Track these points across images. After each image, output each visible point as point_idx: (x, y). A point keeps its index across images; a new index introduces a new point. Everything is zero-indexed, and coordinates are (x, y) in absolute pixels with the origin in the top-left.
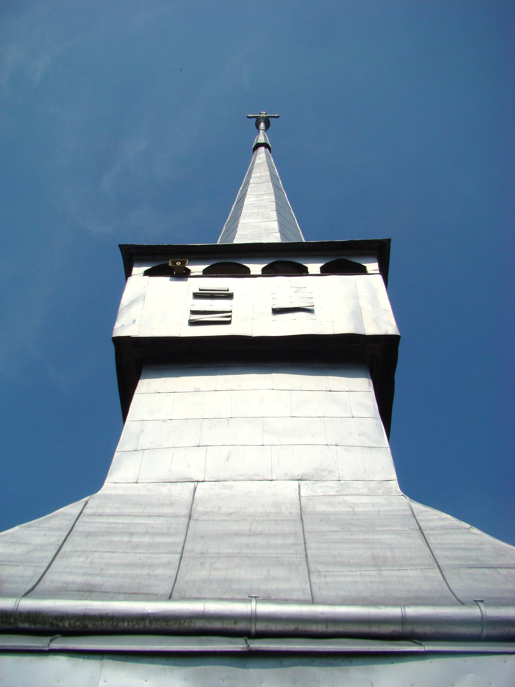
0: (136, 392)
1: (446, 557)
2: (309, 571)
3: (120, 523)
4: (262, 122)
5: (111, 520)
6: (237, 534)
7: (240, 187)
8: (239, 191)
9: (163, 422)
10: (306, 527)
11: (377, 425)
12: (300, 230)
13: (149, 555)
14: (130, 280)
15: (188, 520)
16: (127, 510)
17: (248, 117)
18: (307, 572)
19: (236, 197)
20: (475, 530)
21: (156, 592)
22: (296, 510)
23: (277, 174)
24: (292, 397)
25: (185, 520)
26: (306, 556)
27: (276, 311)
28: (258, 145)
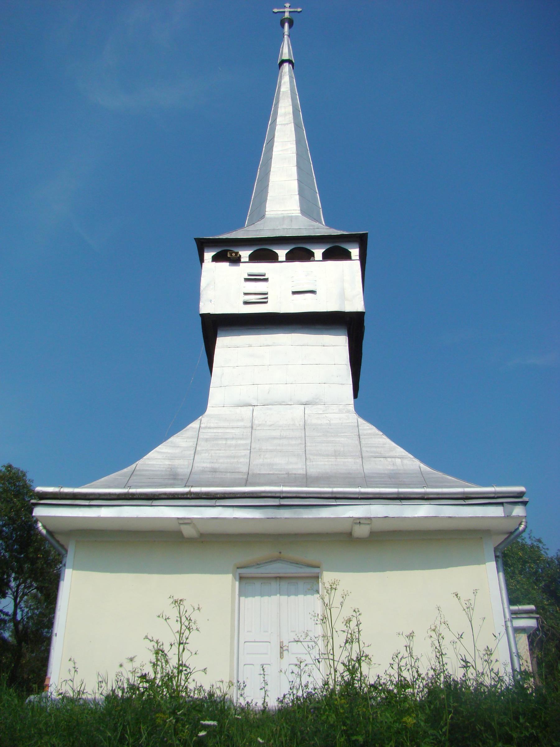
0: (216, 347)
1: (367, 451)
5: (215, 431)
6: (274, 438)
8: (269, 125)
9: (233, 368)
10: (306, 433)
13: (236, 451)
14: (204, 265)
16: (222, 424)
18: (305, 459)
20: (384, 437)
21: (242, 471)
22: (302, 423)
25: (250, 430)
26: (305, 451)
27: (294, 293)
28: (283, 62)
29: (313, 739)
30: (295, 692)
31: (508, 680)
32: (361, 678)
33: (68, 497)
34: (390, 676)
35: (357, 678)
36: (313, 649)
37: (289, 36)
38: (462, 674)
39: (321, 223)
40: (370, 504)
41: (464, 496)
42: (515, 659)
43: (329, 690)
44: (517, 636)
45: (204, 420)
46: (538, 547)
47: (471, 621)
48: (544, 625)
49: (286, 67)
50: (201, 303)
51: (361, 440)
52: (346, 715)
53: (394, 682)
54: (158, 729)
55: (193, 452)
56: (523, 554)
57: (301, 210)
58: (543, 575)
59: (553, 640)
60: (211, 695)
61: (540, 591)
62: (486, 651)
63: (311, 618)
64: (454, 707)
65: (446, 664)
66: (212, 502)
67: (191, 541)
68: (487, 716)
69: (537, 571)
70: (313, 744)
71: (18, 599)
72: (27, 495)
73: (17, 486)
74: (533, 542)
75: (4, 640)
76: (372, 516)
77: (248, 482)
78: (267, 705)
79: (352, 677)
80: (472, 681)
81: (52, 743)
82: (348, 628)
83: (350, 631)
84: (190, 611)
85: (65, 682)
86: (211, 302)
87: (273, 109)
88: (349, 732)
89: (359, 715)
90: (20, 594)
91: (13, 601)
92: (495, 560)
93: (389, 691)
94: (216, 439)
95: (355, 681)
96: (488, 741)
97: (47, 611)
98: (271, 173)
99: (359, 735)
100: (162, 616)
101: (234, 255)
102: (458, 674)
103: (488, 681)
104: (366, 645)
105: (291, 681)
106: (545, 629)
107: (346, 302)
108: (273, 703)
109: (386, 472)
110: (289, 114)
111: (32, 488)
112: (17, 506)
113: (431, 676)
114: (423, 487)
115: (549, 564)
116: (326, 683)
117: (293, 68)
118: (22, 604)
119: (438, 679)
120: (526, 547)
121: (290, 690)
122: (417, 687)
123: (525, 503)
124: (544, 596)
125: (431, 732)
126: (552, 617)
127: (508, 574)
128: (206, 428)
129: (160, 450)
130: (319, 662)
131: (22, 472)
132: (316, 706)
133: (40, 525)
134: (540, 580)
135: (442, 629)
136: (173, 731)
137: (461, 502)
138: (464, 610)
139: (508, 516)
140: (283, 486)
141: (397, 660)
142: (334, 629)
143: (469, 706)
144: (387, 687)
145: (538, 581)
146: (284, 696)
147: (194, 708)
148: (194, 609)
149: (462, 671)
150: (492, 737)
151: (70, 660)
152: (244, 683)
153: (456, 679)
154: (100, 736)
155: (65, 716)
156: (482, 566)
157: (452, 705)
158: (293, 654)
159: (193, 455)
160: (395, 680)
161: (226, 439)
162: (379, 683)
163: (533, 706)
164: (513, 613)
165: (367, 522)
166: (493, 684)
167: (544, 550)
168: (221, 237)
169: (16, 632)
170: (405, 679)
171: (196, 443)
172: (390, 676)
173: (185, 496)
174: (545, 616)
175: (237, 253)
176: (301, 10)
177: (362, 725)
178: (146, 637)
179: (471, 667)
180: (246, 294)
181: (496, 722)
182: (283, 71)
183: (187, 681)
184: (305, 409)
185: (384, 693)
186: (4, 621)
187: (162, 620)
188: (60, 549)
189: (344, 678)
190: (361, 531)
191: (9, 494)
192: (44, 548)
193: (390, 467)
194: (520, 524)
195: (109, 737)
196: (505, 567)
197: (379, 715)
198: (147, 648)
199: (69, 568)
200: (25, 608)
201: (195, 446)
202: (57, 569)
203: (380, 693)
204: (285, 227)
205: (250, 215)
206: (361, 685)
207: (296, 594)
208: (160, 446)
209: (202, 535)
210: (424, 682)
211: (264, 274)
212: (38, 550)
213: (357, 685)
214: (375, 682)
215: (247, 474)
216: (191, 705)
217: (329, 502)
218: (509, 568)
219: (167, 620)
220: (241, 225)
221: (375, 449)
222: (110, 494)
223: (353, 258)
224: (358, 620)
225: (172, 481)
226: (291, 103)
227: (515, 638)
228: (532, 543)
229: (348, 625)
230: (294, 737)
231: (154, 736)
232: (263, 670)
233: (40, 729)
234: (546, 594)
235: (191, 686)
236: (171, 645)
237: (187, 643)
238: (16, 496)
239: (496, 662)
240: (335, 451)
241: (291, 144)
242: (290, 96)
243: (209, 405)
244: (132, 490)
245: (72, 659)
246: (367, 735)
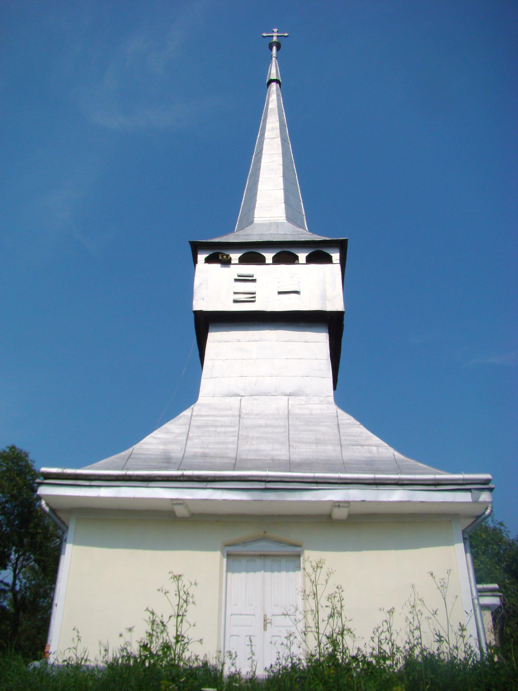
0: (207, 341)
2: (289, 446)
3: (210, 420)
4: (274, 46)
5: (206, 418)
6: (261, 426)
7: (258, 134)
8: (257, 139)
9: (223, 361)
10: (290, 422)
11: (328, 364)
12: (299, 187)
14: (198, 266)
15: (239, 418)
16: (213, 413)
18: (288, 447)
19: (255, 147)
20: (361, 426)
23: (284, 119)
25: (238, 418)
26: (289, 438)
27: (280, 293)
28: (271, 81)
36: (299, 622)
37: (277, 58)
39: (304, 229)
40: (349, 489)
41: (436, 482)
45: (196, 408)
46: (500, 530)
47: (444, 599)
48: (505, 602)
49: (274, 86)
50: (194, 301)
51: (340, 430)
55: (185, 438)
57: (287, 217)
58: (505, 556)
59: (514, 617)
60: (205, 664)
61: (502, 571)
63: (298, 594)
64: (431, 678)
66: (203, 485)
69: (499, 552)
71: (17, 571)
73: (20, 466)
74: (495, 525)
75: (3, 608)
76: (350, 500)
77: (236, 466)
80: (445, 654)
84: (188, 585)
86: (203, 300)
87: (261, 124)
90: (19, 566)
91: (12, 573)
92: (463, 542)
94: (206, 426)
98: (260, 183)
100: (162, 590)
101: (225, 257)
102: (432, 647)
104: (348, 619)
106: (506, 607)
107: (327, 302)
108: (261, 673)
109: (363, 459)
110: (276, 129)
112: (20, 484)
114: (398, 474)
115: (510, 546)
117: (280, 87)
118: (21, 576)
120: (489, 530)
121: (276, 660)
123: (491, 490)
124: (505, 575)
126: (513, 595)
128: (197, 416)
129: (155, 436)
131: (25, 453)
133: (43, 502)
138: (438, 588)
139: (476, 502)
140: (269, 471)
141: (377, 634)
145: (499, 561)
148: (191, 584)
149: (436, 645)
151: (74, 629)
152: (236, 653)
156: (451, 547)
158: (275, 626)
159: (186, 441)
160: (376, 652)
161: (216, 426)
163: (504, 679)
164: (479, 591)
165: (345, 505)
167: (505, 533)
168: (213, 241)
169: (15, 602)
170: (385, 651)
171: (188, 429)
173: (178, 479)
174: (507, 594)
175: (228, 256)
176: (288, 35)
178: (147, 609)
179: (445, 642)
180: (235, 293)
182: (271, 90)
184: (288, 400)
186: (4, 591)
187: (161, 594)
190: (340, 514)
191: (12, 473)
192: (44, 524)
193: (367, 455)
194: (487, 509)
197: (362, 685)
198: (446, 647)
199: (70, 543)
201: (188, 432)
204: (271, 232)
205: (239, 221)
207: (279, 571)
208: (155, 432)
209: (193, 515)
211: (252, 275)
212: (37, 526)
215: (235, 459)
220: (231, 230)
221: (352, 438)
222: (109, 476)
223: (334, 262)
224: (341, 596)
225: (166, 465)
226: (278, 119)
228: (494, 526)
232: (251, 641)
234: (507, 574)
238: (18, 475)
239: (470, 637)
240: (316, 439)
241: (277, 156)
242: (277, 112)
243: (201, 394)
244: (130, 473)
245: (76, 629)
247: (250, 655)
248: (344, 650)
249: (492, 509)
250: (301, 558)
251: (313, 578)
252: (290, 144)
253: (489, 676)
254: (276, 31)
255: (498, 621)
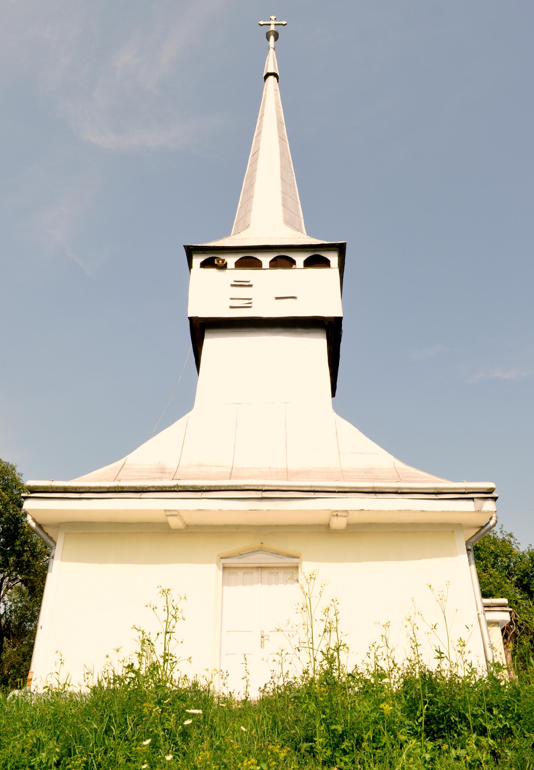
17: (260, 24)
24: (164, 610)
27: (277, 298)
28: (268, 75)
29: (294, 728)
30: (276, 680)
31: (482, 673)
32: (339, 668)
33: (59, 490)
34: (368, 665)
35: (335, 667)
38: (437, 666)
41: (436, 491)
42: (489, 650)
43: (309, 679)
44: (490, 630)
46: (510, 542)
47: (444, 612)
48: (517, 619)
52: (326, 703)
53: (372, 672)
54: (144, 719)
56: (495, 548)
60: (195, 684)
62: (459, 642)
65: (421, 655)
66: (198, 495)
67: (178, 532)
68: (461, 707)
70: (294, 733)
72: (15, 488)
78: (249, 695)
79: (331, 666)
80: (446, 672)
81: (38, 737)
82: (327, 617)
83: (328, 621)
85: (51, 675)
88: (328, 721)
89: (337, 704)
93: (366, 681)
95: (333, 670)
96: (463, 732)
97: (31, 604)
99: (338, 724)
101: (220, 262)
102: (432, 665)
103: (462, 673)
104: (344, 634)
105: (272, 670)
106: (519, 623)
111: (21, 482)
112: (5, 499)
113: (407, 667)
115: (521, 559)
116: (306, 672)
117: (278, 82)
119: (414, 670)
121: (271, 680)
122: (393, 677)
123: (495, 499)
125: (407, 722)
126: (525, 611)
127: (481, 567)
130: (299, 650)
131: (11, 466)
132: (296, 695)
133: (29, 518)
134: (512, 574)
135: (417, 620)
136: (159, 721)
137: (434, 496)
138: (437, 601)
141: (373, 649)
142: (313, 618)
143: (444, 697)
144: (365, 676)
146: (266, 685)
147: (179, 698)
150: (466, 728)
153: (431, 670)
154: (86, 728)
155: (49, 710)
157: (427, 695)
160: (372, 670)
162: (357, 672)
163: (505, 698)
165: (344, 514)
166: (466, 675)
167: (515, 545)
172: (368, 665)
173: (173, 489)
175: (223, 261)
176: (286, 23)
177: (341, 715)
179: (445, 658)
181: (470, 714)
183: (172, 671)
185: (362, 683)
187: (150, 610)
188: (49, 541)
189: (323, 667)
190: (339, 523)
194: (491, 519)
195: (95, 728)
196: (477, 560)
197: (357, 705)
200: (8, 602)
202: (44, 562)
203: (358, 683)
206: (339, 674)
209: (188, 526)
210: (400, 672)
213: (336, 674)
214: (353, 672)
216: (176, 695)
217: (309, 495)
218: (482, 561)
219: (155, 609)
220: (227, 234)
225: (160, 475)
227: (488, 631)
229: (327, 615)
230: (275, 726)
231: (140, 726)
232: (246, 659)
233: (26, 724)
234: (519, 589)
235: (176, 676)
236: (158, 634)
237: (174, 632)
245: (59, 652)
246: (346, 725)
247: (245, 674)
248: (340, 667)
249: (497, 519)
250: (300, 569)
251: (306, 591)
252: (288, 142)
253: (491, 695)
254: (274, 19)
255: (510, 638)
